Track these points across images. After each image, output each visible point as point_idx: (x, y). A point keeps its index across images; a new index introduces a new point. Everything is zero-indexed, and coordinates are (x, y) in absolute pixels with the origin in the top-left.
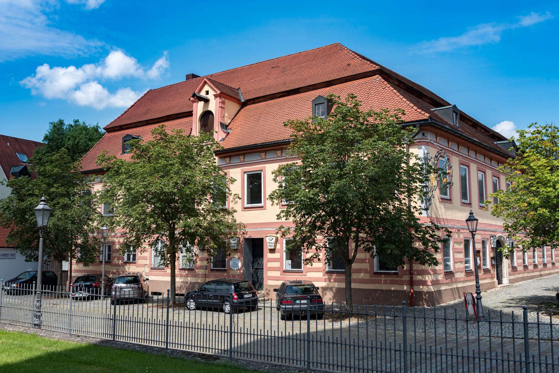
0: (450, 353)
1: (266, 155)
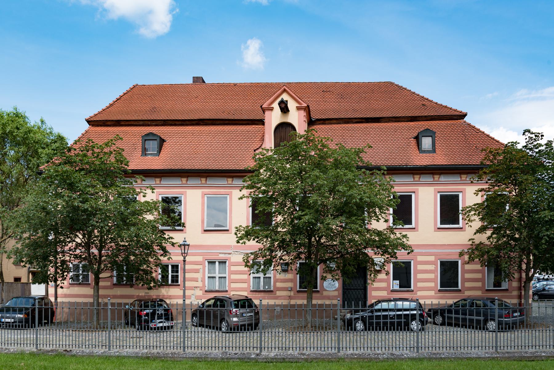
0: (125, 344)
1: (187, 181)
